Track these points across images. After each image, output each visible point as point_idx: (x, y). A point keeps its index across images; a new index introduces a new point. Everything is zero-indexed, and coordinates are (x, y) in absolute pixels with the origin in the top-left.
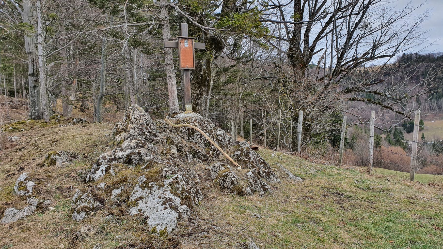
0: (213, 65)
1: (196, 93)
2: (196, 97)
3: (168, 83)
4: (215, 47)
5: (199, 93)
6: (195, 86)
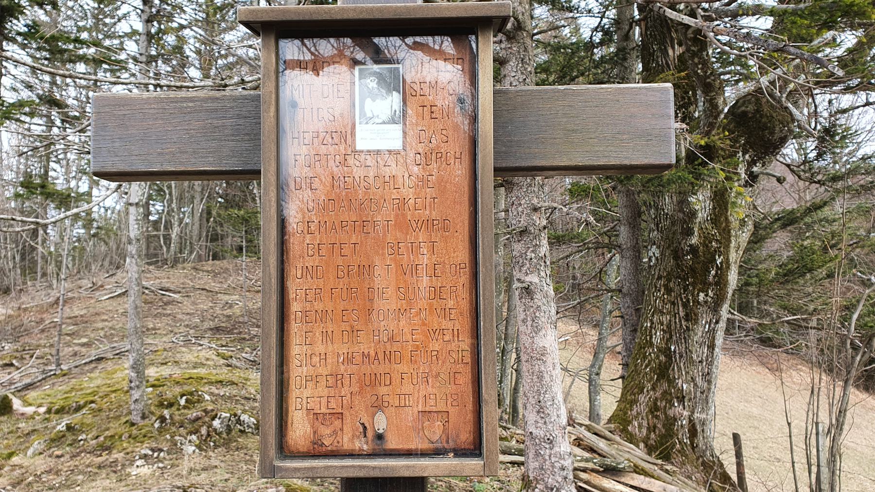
0: (736, 215)
1: (669, 313)
2: (669, 326)
3: (520, 313)
4: (747, 142)
5: (682, 314)
6: (666, 287)
